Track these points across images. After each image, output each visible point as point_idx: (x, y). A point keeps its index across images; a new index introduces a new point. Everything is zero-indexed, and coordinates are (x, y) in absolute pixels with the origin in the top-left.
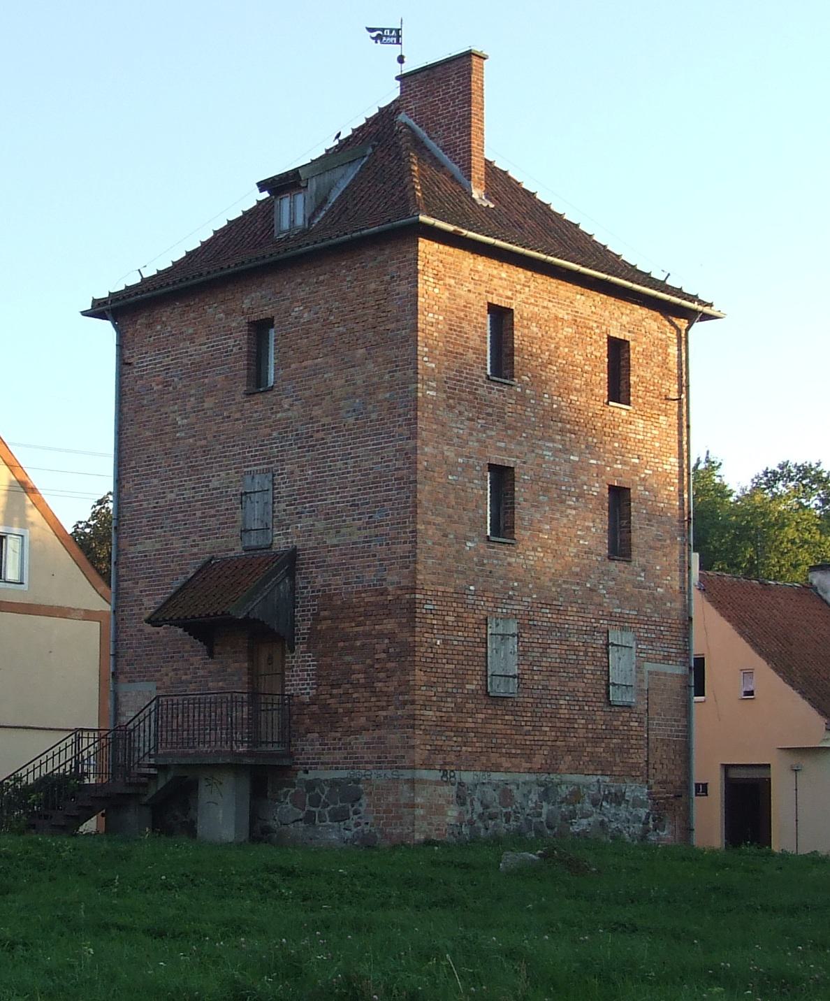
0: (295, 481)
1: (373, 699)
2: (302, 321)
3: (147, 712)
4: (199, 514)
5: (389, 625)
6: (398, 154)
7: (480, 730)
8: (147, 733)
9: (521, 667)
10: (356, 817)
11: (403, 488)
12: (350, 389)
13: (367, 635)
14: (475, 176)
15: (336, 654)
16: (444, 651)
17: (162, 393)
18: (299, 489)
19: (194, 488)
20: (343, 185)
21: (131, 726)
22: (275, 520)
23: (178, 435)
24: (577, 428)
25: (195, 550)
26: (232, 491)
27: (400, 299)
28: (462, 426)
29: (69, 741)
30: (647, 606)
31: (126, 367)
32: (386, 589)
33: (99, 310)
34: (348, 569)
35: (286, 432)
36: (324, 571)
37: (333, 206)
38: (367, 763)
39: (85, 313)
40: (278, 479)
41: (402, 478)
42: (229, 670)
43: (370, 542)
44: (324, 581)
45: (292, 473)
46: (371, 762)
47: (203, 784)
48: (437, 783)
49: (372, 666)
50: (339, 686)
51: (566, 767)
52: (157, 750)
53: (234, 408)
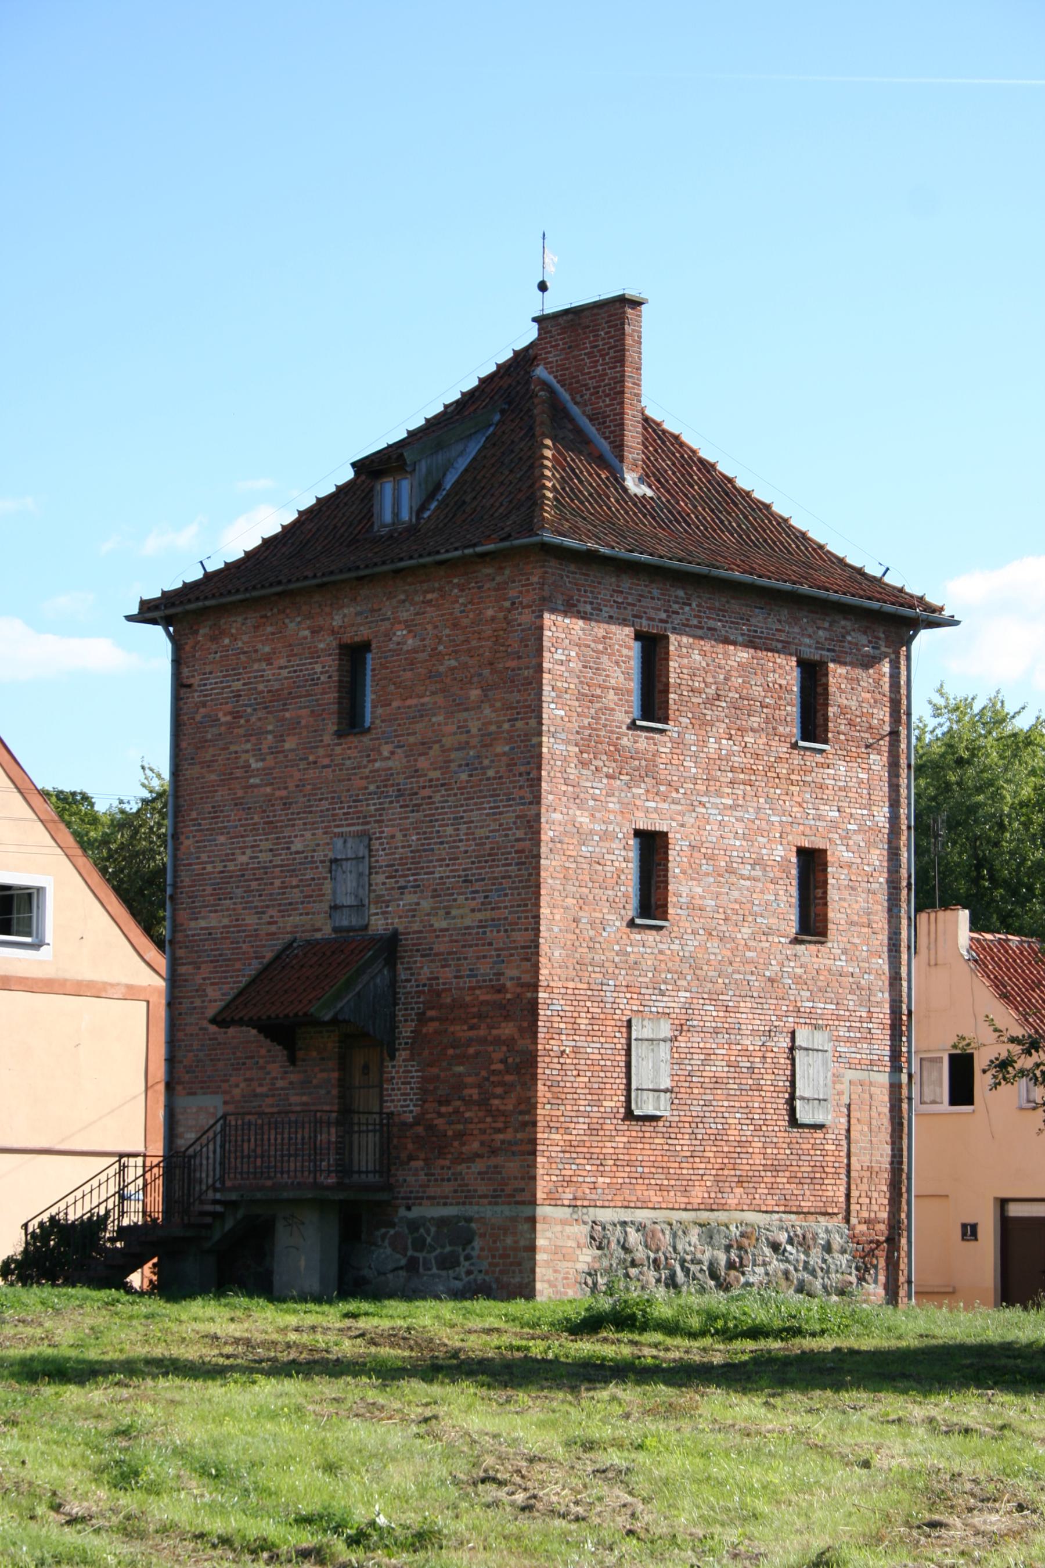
0: (396, 848)
1: (489, 1119)
2: (405, 648)
3: (211, 1134)
4: (277, 883)
5: (507, 1030)
6: (531, 428)
7: (621, 1157)
8: (211, 1161)
9: (676, 1078)
10: (467, 1264)
11: (524, 863)
12: (463, 738)
13: (483, 1041)
14: (629, 456)
15: (444, 1064)
16: (575, 1061)
17: (230, 726)
18: (401, 859)
19: (271, 850)
20: (462, 464)
21: (191, 1151)
22: (372, 895)
23: (252, 781)
24: (753, 778)
25: (273, 928)
26: (319, 856)
27: (523, 630)
28: (600, 785)
29: (111, 1171)
30: (849, 997)
31: (184, 690)
32: (504, 986)
33: (150, 612)
34: (459, 959)
35: (385, 786)
36: (432, 961)
37: (448, 495)
38: (480, 1197)
39: (130, 618)
40: (376, 845)
41: (522, 851)
42: (315, 1082)
43: (485, 927)
44: (432, 973)
45: (393, 837)
46: (485, 1196)
47: (280, 1227)
48: (564, 1222)
49: (487, 1079)
50: (448, 1103)
51: (736, 1201)
52: (223, 1183)
53: (321, 751)
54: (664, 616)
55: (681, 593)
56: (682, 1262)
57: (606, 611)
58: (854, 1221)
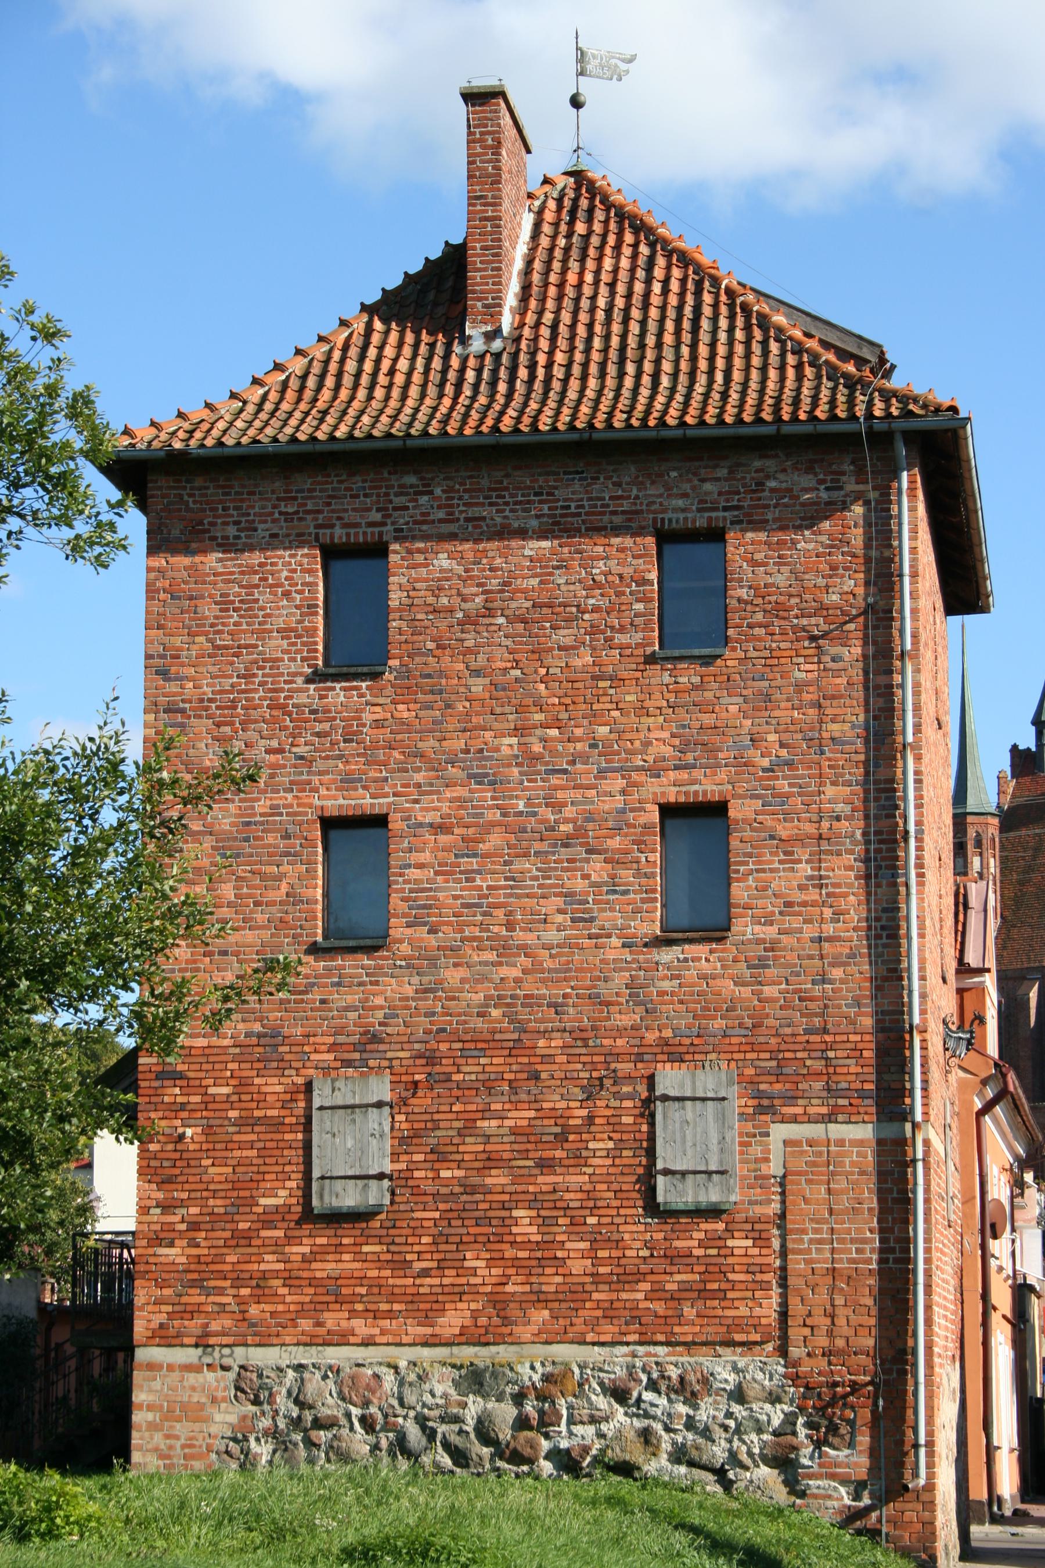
54: (377, 517)
55: (411, 479)
56: (421, 1421)
57: (263, 530)
58: (795, 1352)
